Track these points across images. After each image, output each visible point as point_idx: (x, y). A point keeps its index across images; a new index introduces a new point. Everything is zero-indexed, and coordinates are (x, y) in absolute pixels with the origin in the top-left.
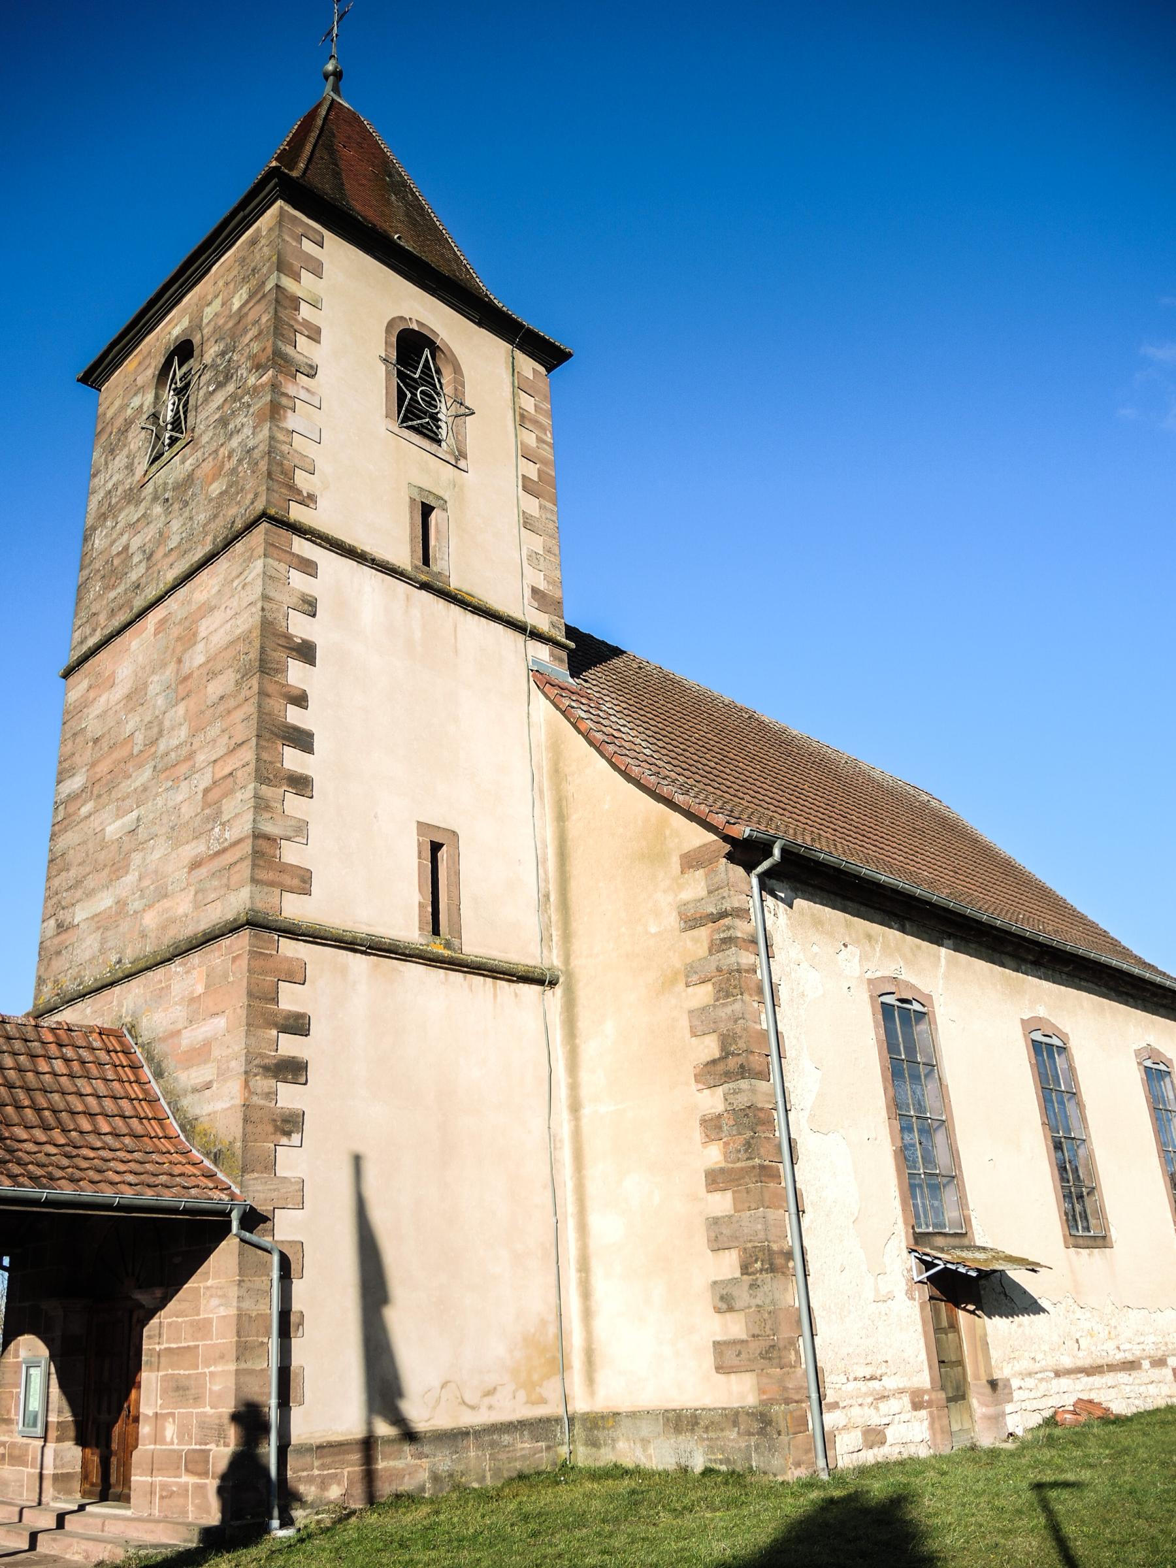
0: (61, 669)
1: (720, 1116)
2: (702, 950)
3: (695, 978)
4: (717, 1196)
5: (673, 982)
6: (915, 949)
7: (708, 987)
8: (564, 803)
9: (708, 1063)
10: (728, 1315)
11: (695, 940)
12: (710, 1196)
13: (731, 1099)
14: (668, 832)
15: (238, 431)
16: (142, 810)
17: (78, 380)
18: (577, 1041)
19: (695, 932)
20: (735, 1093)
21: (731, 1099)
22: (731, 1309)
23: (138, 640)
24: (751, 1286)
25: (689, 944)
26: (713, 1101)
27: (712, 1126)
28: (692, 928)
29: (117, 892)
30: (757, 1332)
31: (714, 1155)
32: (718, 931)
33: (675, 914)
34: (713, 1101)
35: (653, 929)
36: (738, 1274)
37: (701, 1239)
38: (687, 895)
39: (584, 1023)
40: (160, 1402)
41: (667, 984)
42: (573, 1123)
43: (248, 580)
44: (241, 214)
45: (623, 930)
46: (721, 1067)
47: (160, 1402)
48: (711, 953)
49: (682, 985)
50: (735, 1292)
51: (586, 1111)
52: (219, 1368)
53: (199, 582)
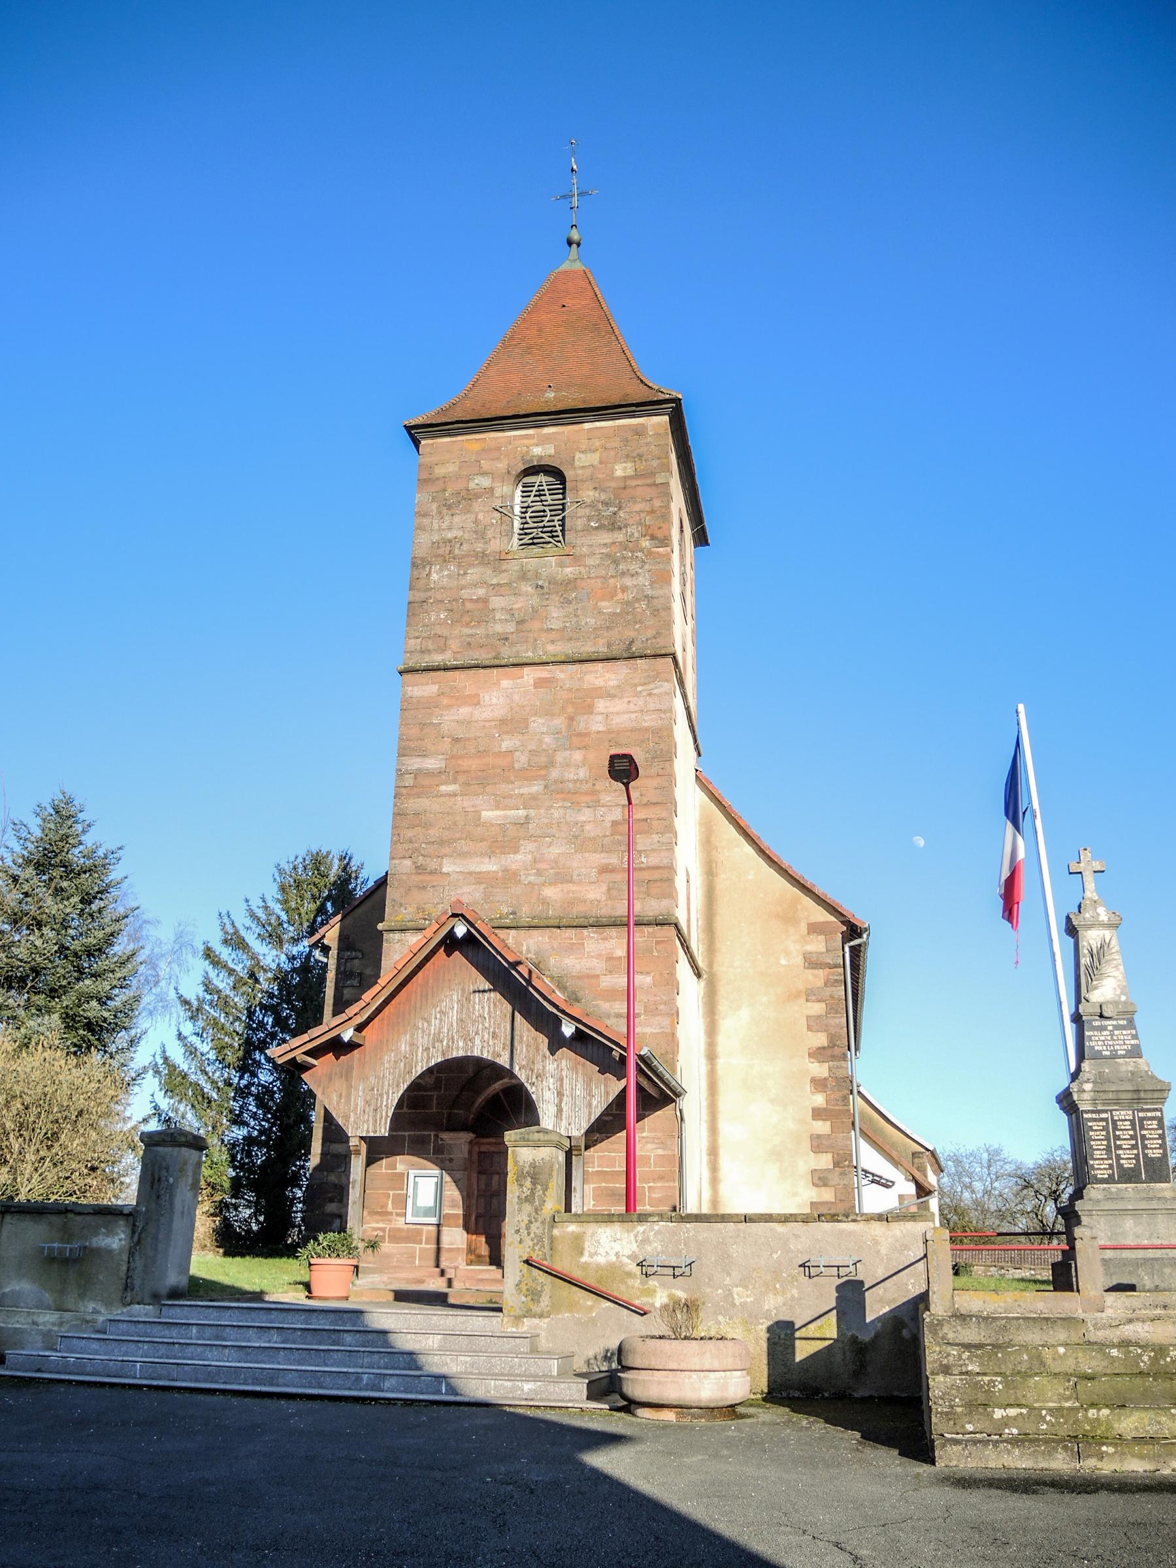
0: (401, 667)
1: (825, 1079)
2: (820, 983)
3: (813, 998)
4: (820, 1123)
5: (797, 996)
6: (348, 908)
7: (823, 1005)
8: (714, 865)
9: (819, 1048)
10: (823, 1189)
11: (816, 976)
12: (814, 1122)
13: (834, 1070)
14: (799, 907)
15: (633, 576)
16: (532, 813)
17: (405, 426)
18: (716, 1017)
19: (816, 971)
20: (837, 1067)
21: (834, 1070)
22: (825, 1185)
23: (511, 682)
24: (841, 1174)
25: (810, 977)
26: (821, 1070)
27: (819, 1084)
28: (813, 968)
29: (503, 862)
30: (843, 1198)
31: (819, 1100)
32: (833, 974)
33: (801, 957)
34: (821, 1070)
35: (783, 962)
36: (831, 1167)
37: (806, 1144)
38: (810, 948)
39: (723, 1006)
40: (592, 1202)
41: (793, 996)
42: (709, 1067)
43: (654, 692)
44: (634, 408)
45: (759, 957)
46: (829, 1052)
47: (592, 1202)
48: (826, 985)
49: (804, 1000)
50: (830, 1176)
51: (721, 1062)
52: (659, 1184)
53: (592, 669)
